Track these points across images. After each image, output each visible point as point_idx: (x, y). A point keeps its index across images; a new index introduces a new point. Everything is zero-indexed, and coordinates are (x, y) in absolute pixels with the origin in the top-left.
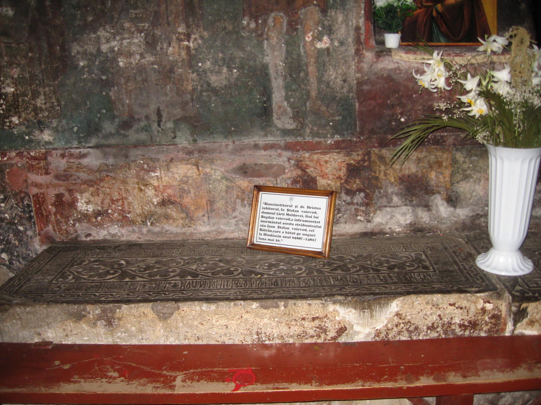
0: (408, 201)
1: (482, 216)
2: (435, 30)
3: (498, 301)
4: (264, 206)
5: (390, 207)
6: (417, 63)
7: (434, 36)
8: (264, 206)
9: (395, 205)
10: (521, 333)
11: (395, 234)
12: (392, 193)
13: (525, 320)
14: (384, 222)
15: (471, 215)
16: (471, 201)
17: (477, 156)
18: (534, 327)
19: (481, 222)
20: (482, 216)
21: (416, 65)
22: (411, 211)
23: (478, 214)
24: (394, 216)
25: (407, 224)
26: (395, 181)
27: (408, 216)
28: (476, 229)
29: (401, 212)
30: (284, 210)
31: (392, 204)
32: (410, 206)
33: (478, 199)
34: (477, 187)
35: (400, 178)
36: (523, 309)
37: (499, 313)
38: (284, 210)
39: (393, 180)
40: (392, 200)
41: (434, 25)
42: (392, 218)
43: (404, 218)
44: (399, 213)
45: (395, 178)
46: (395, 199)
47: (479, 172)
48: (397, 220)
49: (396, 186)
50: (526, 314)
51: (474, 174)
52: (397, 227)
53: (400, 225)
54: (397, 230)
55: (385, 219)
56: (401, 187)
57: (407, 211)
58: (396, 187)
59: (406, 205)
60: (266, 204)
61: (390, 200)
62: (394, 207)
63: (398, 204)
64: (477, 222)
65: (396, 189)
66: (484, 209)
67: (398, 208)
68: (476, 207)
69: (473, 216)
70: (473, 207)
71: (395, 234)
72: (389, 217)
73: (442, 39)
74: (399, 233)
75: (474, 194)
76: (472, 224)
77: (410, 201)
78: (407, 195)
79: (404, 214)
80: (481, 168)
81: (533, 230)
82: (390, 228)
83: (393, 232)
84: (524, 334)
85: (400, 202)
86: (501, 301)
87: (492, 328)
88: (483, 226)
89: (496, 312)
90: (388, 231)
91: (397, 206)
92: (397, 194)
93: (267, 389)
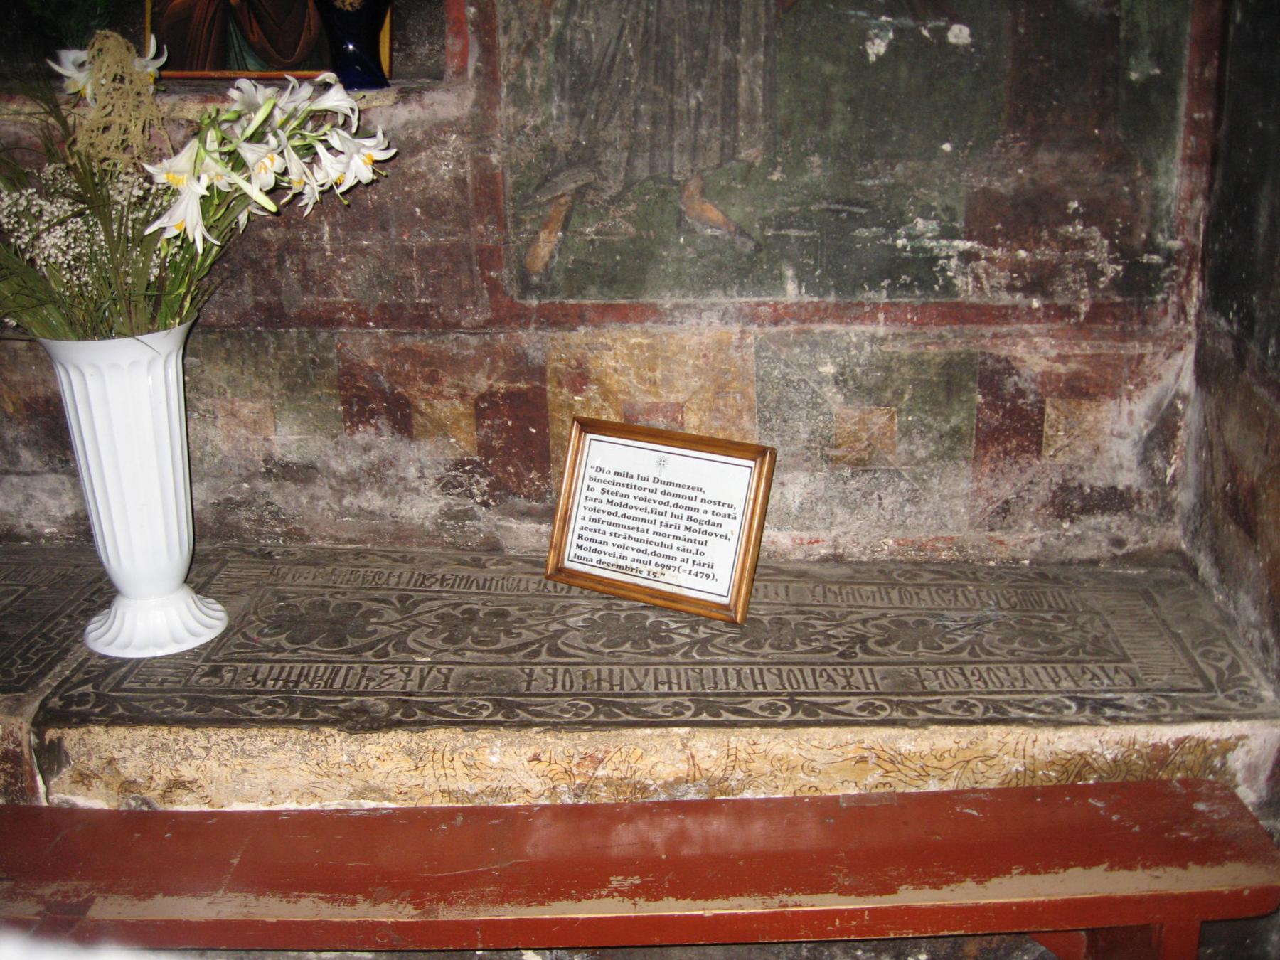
0: (57, 461)
1: (239, 505)
2: (235, 40)
3: (13, 720)
4: (592, 473)
5: (18, 474)
6: (15, 123)
7: (232, 55)
8: (592, 473)
9: (29, 470)
10: (67, 802)
11: (43, 541)
12: (16, 441)
13: (66, 772)
14: (12, 511)
15: (212, 501)
16: (206, 466)
17: (197, 356)
18: (94, 789)
19: (239, 521)
20: (239, 505)
21: (12, 129)
22: (69, 486)
23: (229, 500)
24: (32, 496)
25: (67, 518)
26: (16, 411)
27: (66, 499)
28: (231, 537)
29: (46, 488)
30: (593, 490)
31: (21, 469)
32: (64, 473)
33: (221, 462)
34: (211, 432)
35: (28, 406)
36: (51, 741)
37: (18, 750)
38: (593, 490)
39: (11, 409)
40: (18, 457)
41: (231, 27)
42: (30, 503)
43: (57, 503)
44: (43, 490)
45: (14, 404)
46: (26, 456)
47: (208, 395)
48: (41, 507)
49: (20, 424)
50: (64, 758)
51: (198, 400)
52: (44, 523)
53: (51, 520)
54: (47, 531)
55: (14, 503)
56: (32, 426)
57: (57, 485)
58: (22, 428)
59: (54, 471)
60: (599, 469)
61: (14, 459)
62: (27, 474)
63: (35, 468)
64: (231, 518)
65: (21, 432)
66: (240, 488)
67: (38, 478)
68: (220, 483)
69: (218, 504)
70: (213, 481)
71: (43, 541)
72: (20, 497)
73: (250, 62)
74: (51, 538)
75: (208, 448)
76: (221, 523)
77: (61, 461)
78: (52, 447)
79: (55, 493)
80: (212, 385)
81: (369, 546)
82: (29, 526)
83: (37, 536)
84: (74, 805)
85: (38, 465)
86: (20, 720)
87: (10, 784)
88: (246, 531)
89: (12, 746)
90: (27, 531)
91: (34, 473)
92: (26, 444)
93: (740, 907)
